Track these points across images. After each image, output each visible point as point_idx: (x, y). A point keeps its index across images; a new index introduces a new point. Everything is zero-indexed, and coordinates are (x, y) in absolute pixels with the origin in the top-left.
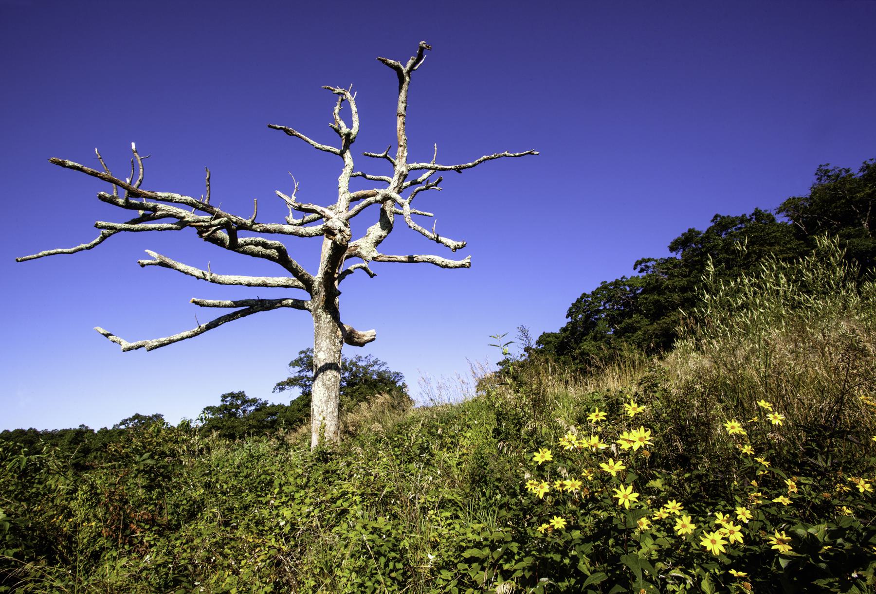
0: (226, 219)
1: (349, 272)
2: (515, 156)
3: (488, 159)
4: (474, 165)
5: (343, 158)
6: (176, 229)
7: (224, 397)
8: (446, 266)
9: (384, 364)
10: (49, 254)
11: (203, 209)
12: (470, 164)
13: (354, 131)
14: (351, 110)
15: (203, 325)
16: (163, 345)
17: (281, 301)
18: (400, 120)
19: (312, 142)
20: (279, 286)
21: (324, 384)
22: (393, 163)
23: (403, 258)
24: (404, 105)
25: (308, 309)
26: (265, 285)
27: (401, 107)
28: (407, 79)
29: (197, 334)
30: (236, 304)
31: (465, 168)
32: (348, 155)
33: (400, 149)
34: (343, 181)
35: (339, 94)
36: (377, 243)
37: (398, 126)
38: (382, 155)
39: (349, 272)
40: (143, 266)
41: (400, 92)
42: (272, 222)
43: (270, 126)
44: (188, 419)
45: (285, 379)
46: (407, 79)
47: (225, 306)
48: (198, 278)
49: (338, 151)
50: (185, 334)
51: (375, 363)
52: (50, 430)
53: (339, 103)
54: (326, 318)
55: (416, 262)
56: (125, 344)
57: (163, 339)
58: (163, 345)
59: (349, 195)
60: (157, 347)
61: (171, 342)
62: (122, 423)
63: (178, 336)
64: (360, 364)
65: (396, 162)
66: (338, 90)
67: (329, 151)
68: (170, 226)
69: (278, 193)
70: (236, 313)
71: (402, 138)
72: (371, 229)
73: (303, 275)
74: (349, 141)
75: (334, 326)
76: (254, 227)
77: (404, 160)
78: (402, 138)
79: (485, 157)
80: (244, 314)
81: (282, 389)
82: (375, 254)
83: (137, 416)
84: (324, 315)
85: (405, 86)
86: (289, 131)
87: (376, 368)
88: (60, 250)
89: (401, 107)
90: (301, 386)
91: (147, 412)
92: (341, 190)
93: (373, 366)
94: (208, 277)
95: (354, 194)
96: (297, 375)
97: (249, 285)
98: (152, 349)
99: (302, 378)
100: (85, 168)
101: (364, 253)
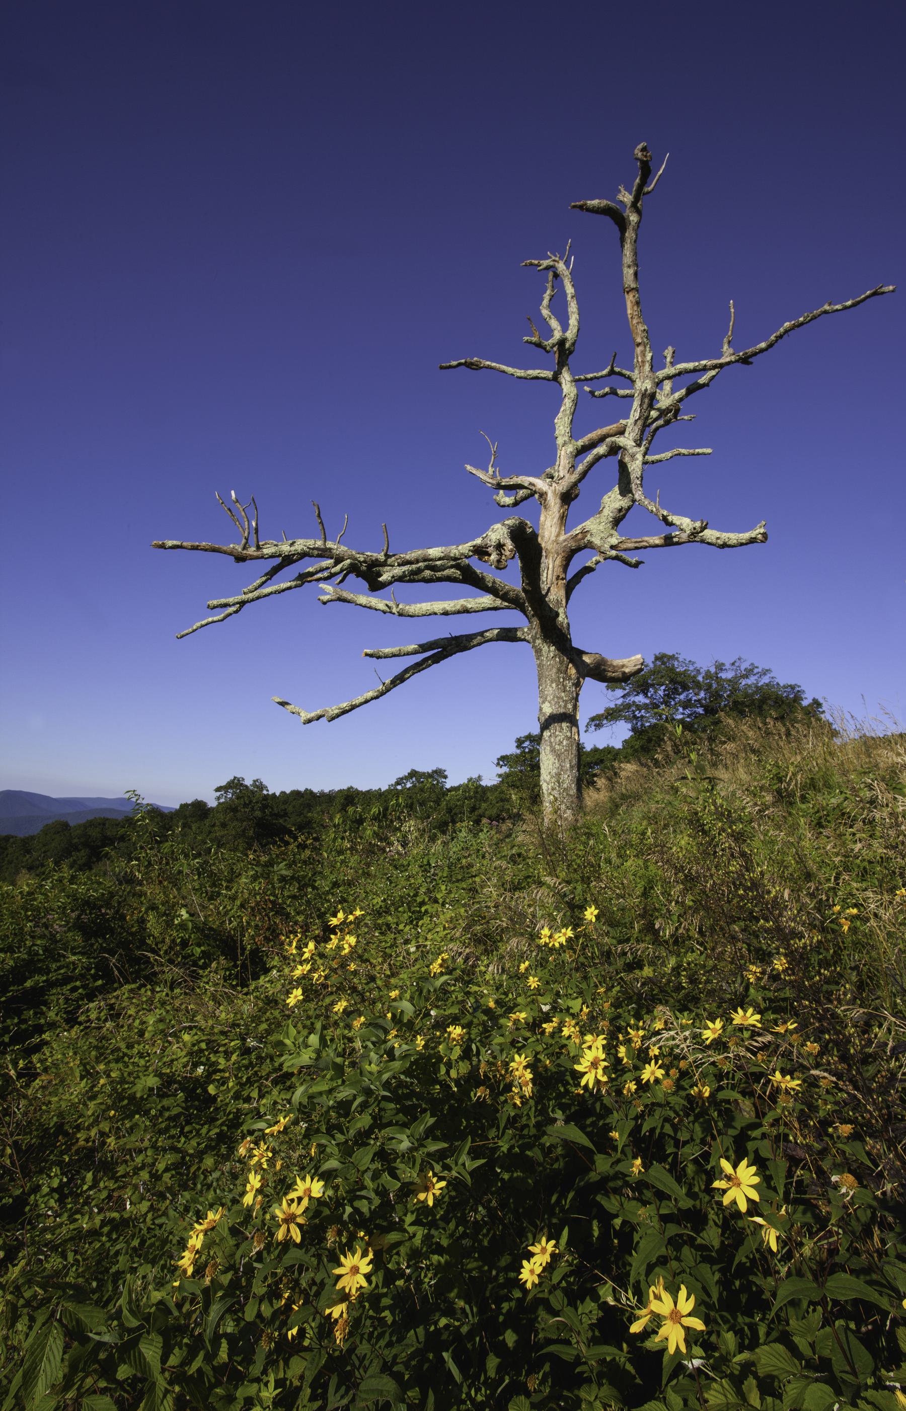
0: (348, 561)
1: (588, 570)
2: (846, 308)
3: (792, 328)
4: (770, 346)
5: (560, 384)
6: (296, 586)
7: (520, 742)
8: (725, 546)
9: (765, 672)
10: (202, 626)
11: (319, 556)
12: (763, 345)
13: (571, 334)
14: (565, 295)
15: (388, 681)
16: (344, 712)
17: (482, 634)
18: (630, 299)
19: (510, 370)
20: (484, 610)
21: (553, 750)
22: (629, 378)
23: (657, 540)
24: (631, 271)
25: (524, 640)
26: (466, 611)
27: (628, 274)
28: (633, 218)
29: (382, 694)
30: (424, 648)
31: (755, 354)
32: (566, 377)
33: (639, 350)
34: (562, 424)
35: (548, 268)
36: (617, 522)
37: (629, 311)
38: (605, 372)
39: (588, 570)
40: (325, 603)
41: (622, 246)
42: (411, 549)
43: (442, 368)
44: (475, 776)
45: (601, 711)
46: (633, 218)
47: (408, 654)
48: (384, 612)
49: (549, 374)
50: (370, 694)
51: (749, 672)
52: (326, 791)
53: (549, 285)
54: (548, 651)
55: (678, 543)
56: (305, 715)
57: (345, 705)
58: (344, 712)
59: (570, 448)
60: (338, 716)
61: (353, 707)
62: (398, 783)
63: (361, 699)
64: (723, 675)
65: (635, 375)
66: (545, 263)
67: (537, 378)
68: (289, 584)
69: (469, 467)
70: (425, 660)
71: (639, 329)
72: (606, 499)
73: (506, 593)
74: (564, 352)
75: (561, 662)
76: (389, 561)
77: (647, 367)
78: (639, 329)
79: (787, 324)
80: (436, 659)
81: (598, 726)
82: (614, 541)
83: (413, 774)
84: (545, 648)
85: (630, 234)
86: (472, 364)
87: (752, 680)
88: (210, 619)
89: (628, 274)
90: (627, 719)
91: (426, 767)
92: (560, 441)
93: (746, 676)
94: (394, 610)
95: (580, 443)
96: (620, 702)
97: (446, 613)
98: (332, 719)
99: (627, 707)
100: (185, 544)
101: (597, 541)
